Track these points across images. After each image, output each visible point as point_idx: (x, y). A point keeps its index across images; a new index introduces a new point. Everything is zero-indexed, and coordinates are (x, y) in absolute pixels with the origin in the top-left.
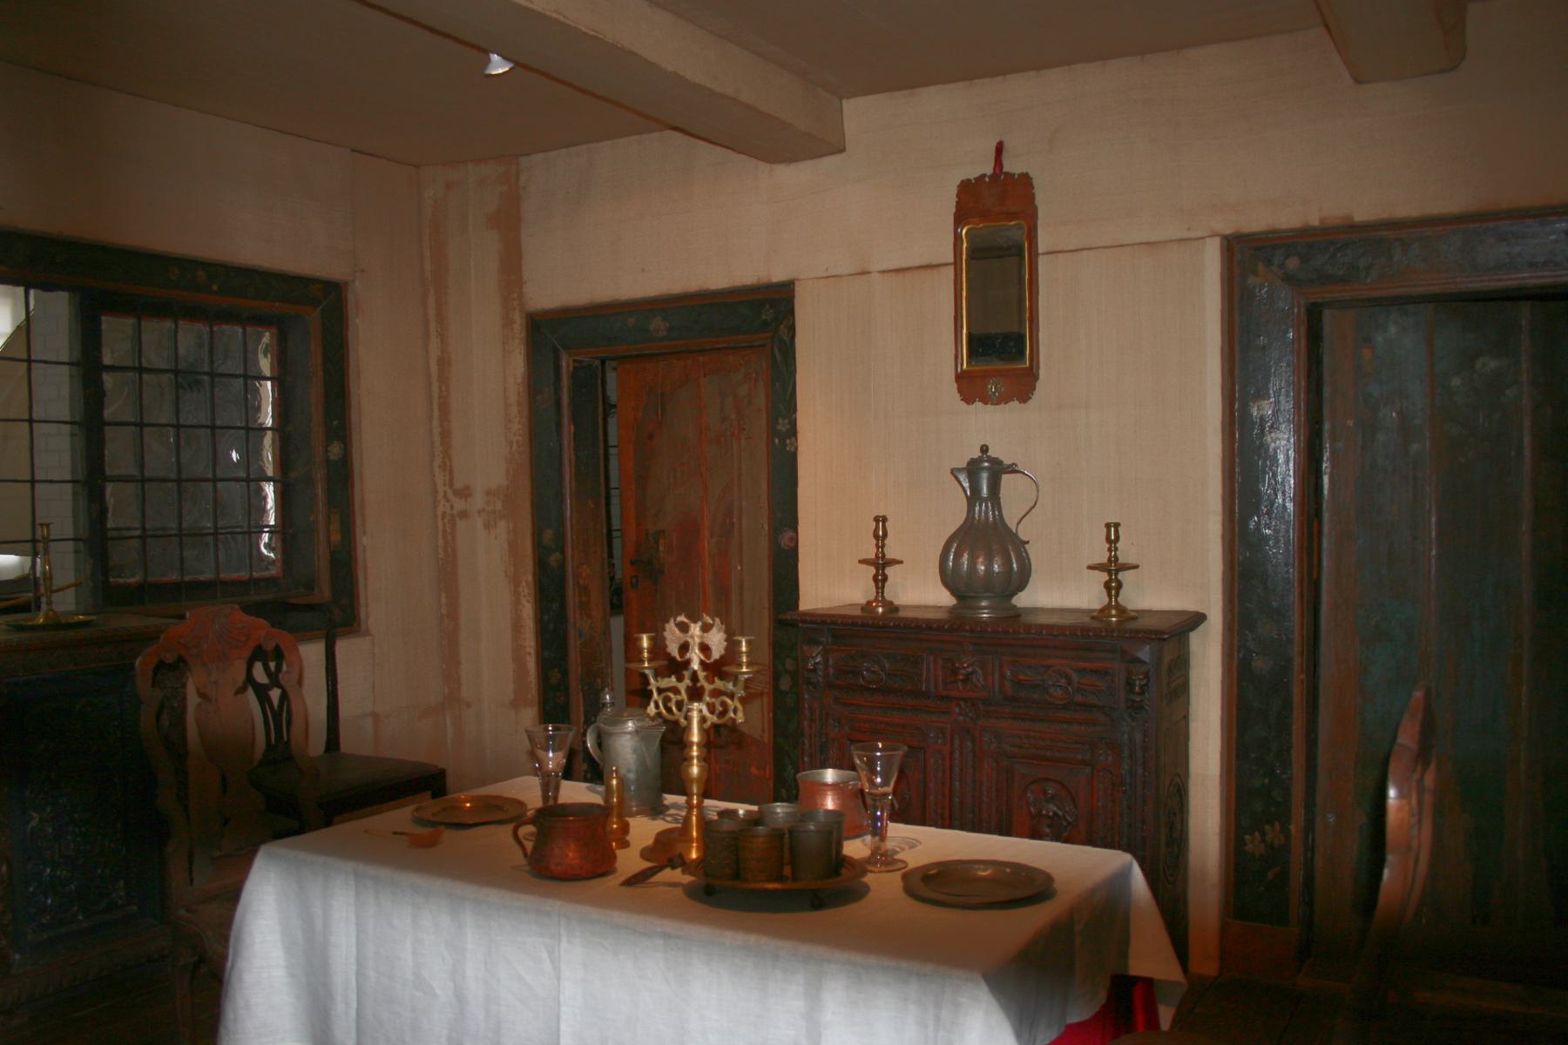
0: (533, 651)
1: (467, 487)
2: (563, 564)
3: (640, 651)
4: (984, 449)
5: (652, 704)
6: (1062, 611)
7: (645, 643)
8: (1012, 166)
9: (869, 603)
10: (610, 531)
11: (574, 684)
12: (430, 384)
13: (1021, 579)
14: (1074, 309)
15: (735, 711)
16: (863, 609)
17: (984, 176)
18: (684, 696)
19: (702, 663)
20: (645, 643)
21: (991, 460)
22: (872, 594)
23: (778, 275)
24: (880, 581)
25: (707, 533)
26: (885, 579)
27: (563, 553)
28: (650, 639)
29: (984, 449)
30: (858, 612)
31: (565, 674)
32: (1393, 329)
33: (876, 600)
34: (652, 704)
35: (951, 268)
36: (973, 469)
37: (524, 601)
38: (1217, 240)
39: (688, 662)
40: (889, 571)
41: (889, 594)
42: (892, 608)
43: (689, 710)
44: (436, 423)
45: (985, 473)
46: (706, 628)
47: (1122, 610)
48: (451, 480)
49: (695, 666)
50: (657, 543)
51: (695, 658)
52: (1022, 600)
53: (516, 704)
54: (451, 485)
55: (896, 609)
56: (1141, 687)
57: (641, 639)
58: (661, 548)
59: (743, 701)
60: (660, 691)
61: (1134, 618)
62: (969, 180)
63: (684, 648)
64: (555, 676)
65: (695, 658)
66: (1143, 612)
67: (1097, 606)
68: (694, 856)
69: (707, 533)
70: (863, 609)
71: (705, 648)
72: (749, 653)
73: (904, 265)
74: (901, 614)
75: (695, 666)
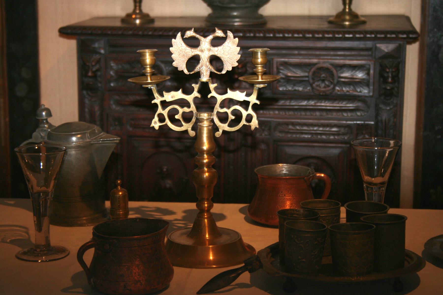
3: (143, 65)
5: (156, 119)
6: (310, 18)
7: (148, 59)
9: (129, 16)
15: (249, 118)
18: (193, 108)
19: (212, 75)
20: (148, 59)
22: (130, 8)
28: (154, 54)
30: (118, 24)
33: (134, 12)
34: (156, 119)
39: (198, 75)
41: (146, 8)
42: (148, 20)
46: (218, 42)
47: (354, 16)
49: (205, 78)
51: (205, 70)
55: (152, 21)
56: (393, 78)
57: (142, 55)
59: (255, 107)
60: (165, 104)
61: (364, 22)
63: (194, 61)
65: (205, 70)
67: (334, 13)
68: (211, 258)
71: (215, 60)
72: (264, 65)
74: (157, 24)
75: (205, 78)
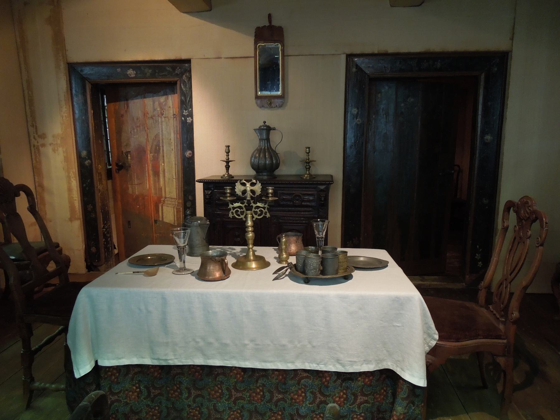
0: (77, 199)
1: (44, 134)
2: (91, 165)
4: (265, 122)
8: (275, 23)
10: (108, 152)
11: (99, 210)
12: (23, 91)
13: (277, 166)
14: (297, 75)
16: (222, 177)
17: (265, 26)
18: (244, 209)
19: (251, 197)
21: (266, 126)
23: (184, 57)
24: (228, 167)
25: (149, 152)
26: (229, 166)
27: (91, 160)
29: (265, 122)
30: (220, 178)
31: (94, 206)
32: (387, 88)
35: (253, 59)
36: (260, 130)
37: (72, 180)
38: (345, 55)
40: (230, 164)
43: (246, 214)
44: (27, 108)
45: (266, 130)
48: (36, 131)
49: (248, 198)
50: (127, 156)
52: (277, 172)
53: (71, 220)
54: (37, 134)
58: (129, 158)
62: (259, 27)
64: (90, 207)
66: (318, 175)
69: (149, 152)
70: (222, 177)
73: (235, 56)
75: (248, 198)
